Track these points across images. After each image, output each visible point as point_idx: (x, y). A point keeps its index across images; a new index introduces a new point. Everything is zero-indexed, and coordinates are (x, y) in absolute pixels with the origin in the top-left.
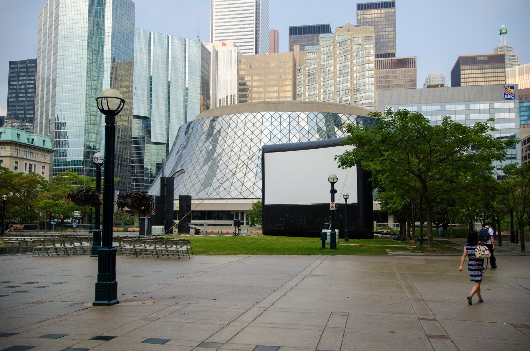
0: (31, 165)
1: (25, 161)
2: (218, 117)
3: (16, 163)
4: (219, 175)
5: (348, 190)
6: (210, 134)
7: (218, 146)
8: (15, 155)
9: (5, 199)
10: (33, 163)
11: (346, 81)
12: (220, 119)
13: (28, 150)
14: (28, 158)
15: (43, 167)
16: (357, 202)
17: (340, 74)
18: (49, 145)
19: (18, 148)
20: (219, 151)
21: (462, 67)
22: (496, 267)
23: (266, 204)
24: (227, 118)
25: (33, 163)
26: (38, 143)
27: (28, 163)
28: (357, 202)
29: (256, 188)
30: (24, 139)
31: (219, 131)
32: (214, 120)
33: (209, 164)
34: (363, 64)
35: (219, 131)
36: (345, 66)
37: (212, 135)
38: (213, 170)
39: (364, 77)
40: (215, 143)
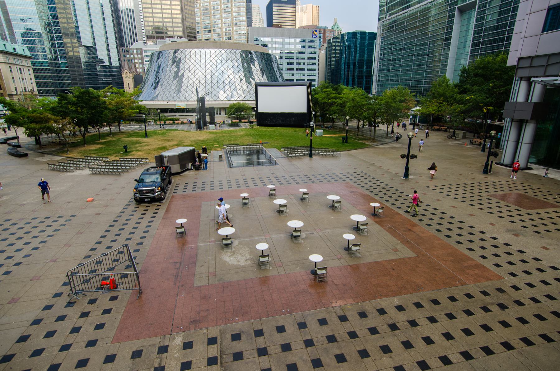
0: (20, 69)
1: (16, 66)
2: (178, 50)
3: (10, 67)
4: (184, 87)
5: (302, 108)
6: (174, 62)
7: (181, 69)
8: (7, 61)
9: (493, 135)
10: (22, 67)
11: (228, 17)
12: (179, 52)
13: (15, 57)
14: (17, 63)
15: (29, 70)
16: (306, 112)
17: (225, 12)
18: (28, 53)
19: (8, 56)
20: (182, 72)
21: (274, 5)
22: (40, 184)
23: (260, 110)
24: (184, 51)
25: (22, 67)
26: (19, 51)
27: (18, 67)
28: (306, 112)
29: (193, 95)
30: (10, 49)
31: (180, 59)
32: (175, 52)
33: (177, 79)
34: (239, 7)
35: (180, 59)
36: (228, 7)
37: (177, 63)
38: (180, 84)
39: (239, 16)
40: (178, 67)
